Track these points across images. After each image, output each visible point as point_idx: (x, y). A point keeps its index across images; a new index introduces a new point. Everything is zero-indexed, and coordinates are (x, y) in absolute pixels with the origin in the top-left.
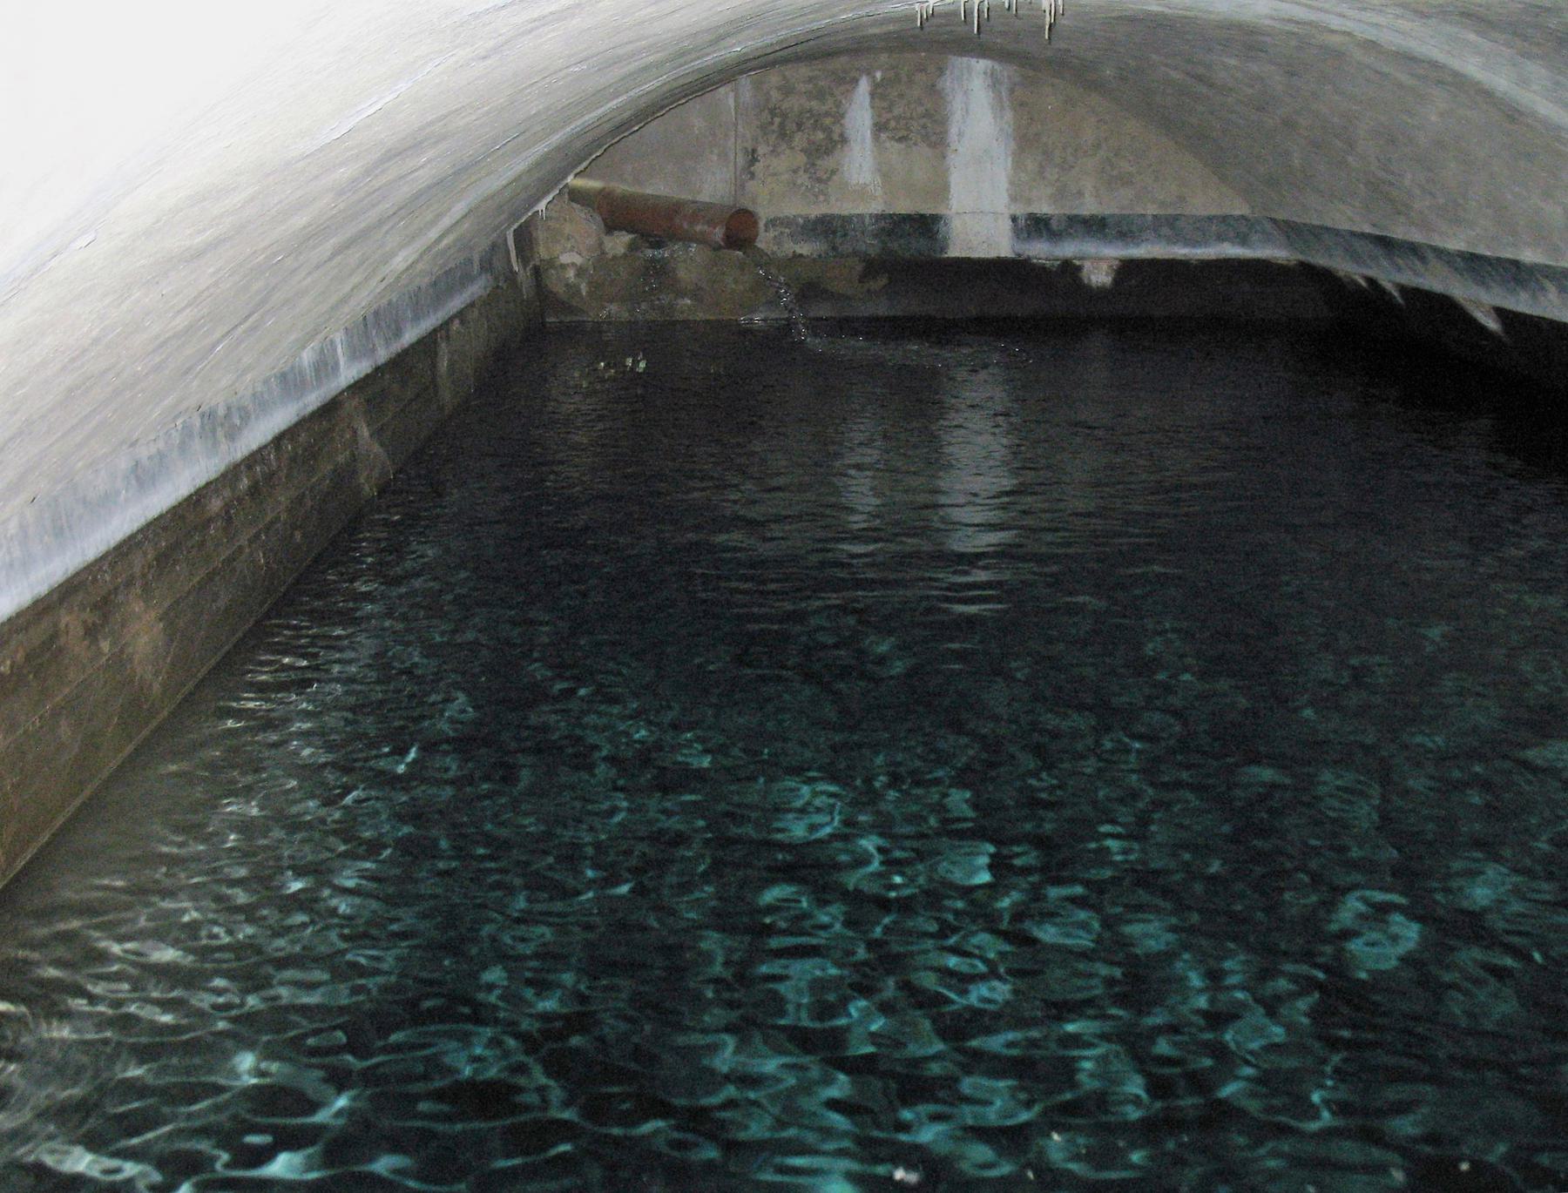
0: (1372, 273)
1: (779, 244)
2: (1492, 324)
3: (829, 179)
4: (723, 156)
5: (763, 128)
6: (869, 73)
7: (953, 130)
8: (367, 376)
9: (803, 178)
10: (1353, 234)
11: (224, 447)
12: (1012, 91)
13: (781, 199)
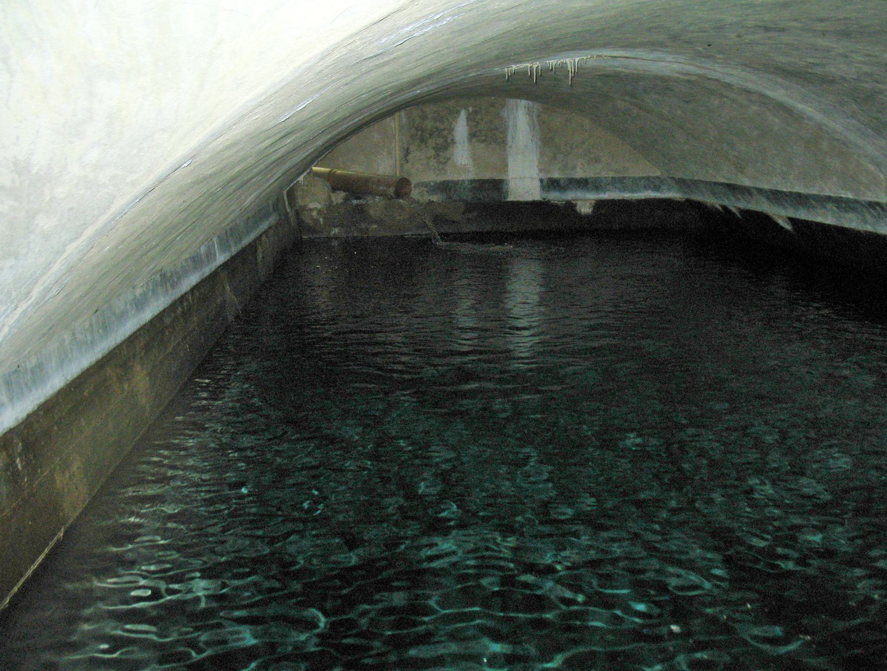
0: (726, 203)
1: (422, 196)
2: (788, 227)
3: (446, 163)
4: (389, 153)
5: (412, 136)
6: (466, 108)
7: (509, 138)
8: (228, 261)
9: (433, 163)
10: (715, 183)
11: (170, 291)
12: (538, 116)
13: (423, 174)
